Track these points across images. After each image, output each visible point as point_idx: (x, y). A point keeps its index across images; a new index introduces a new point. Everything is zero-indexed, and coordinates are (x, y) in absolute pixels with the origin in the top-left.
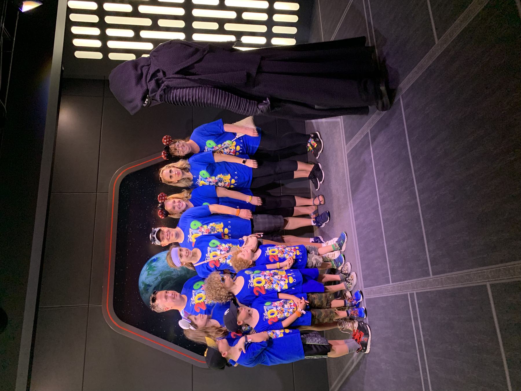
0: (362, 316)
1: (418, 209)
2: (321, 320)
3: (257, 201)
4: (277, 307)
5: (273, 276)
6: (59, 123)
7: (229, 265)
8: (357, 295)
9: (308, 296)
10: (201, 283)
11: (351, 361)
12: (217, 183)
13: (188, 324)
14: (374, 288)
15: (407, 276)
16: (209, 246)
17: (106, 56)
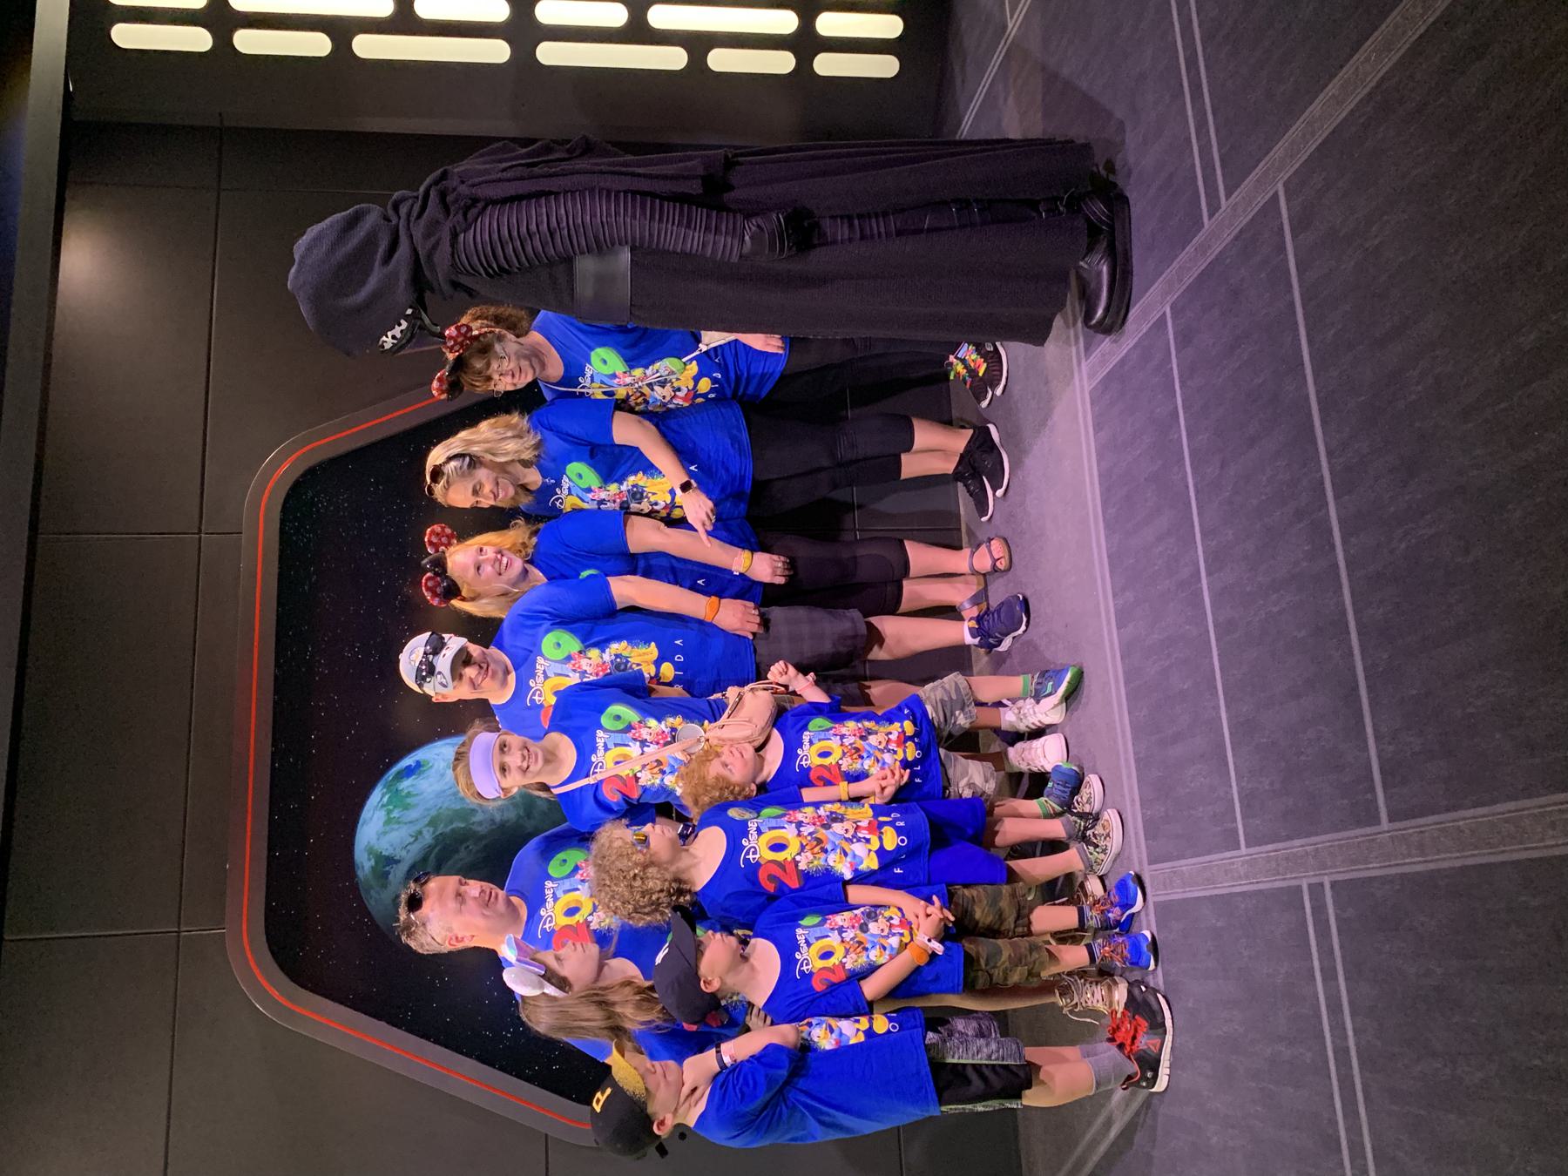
0: (1143, 962)
1: (1340, 587)
2: (997, 974)
3: (769, 571)
4: (841, 930)
5: (827, 827)
6: (61, 286)
7: (671, 793)
8: (1125, 889)
9: (951, 895)
10: (573, 856)
11: (1100, 1120)
12: (625, 507)
13: (535, 978)
14: (1186, 865)
15: (1305, 820)
16: (601, 727)
17: (805, 62)
